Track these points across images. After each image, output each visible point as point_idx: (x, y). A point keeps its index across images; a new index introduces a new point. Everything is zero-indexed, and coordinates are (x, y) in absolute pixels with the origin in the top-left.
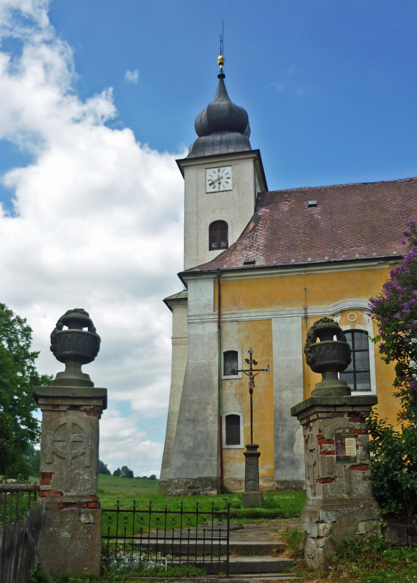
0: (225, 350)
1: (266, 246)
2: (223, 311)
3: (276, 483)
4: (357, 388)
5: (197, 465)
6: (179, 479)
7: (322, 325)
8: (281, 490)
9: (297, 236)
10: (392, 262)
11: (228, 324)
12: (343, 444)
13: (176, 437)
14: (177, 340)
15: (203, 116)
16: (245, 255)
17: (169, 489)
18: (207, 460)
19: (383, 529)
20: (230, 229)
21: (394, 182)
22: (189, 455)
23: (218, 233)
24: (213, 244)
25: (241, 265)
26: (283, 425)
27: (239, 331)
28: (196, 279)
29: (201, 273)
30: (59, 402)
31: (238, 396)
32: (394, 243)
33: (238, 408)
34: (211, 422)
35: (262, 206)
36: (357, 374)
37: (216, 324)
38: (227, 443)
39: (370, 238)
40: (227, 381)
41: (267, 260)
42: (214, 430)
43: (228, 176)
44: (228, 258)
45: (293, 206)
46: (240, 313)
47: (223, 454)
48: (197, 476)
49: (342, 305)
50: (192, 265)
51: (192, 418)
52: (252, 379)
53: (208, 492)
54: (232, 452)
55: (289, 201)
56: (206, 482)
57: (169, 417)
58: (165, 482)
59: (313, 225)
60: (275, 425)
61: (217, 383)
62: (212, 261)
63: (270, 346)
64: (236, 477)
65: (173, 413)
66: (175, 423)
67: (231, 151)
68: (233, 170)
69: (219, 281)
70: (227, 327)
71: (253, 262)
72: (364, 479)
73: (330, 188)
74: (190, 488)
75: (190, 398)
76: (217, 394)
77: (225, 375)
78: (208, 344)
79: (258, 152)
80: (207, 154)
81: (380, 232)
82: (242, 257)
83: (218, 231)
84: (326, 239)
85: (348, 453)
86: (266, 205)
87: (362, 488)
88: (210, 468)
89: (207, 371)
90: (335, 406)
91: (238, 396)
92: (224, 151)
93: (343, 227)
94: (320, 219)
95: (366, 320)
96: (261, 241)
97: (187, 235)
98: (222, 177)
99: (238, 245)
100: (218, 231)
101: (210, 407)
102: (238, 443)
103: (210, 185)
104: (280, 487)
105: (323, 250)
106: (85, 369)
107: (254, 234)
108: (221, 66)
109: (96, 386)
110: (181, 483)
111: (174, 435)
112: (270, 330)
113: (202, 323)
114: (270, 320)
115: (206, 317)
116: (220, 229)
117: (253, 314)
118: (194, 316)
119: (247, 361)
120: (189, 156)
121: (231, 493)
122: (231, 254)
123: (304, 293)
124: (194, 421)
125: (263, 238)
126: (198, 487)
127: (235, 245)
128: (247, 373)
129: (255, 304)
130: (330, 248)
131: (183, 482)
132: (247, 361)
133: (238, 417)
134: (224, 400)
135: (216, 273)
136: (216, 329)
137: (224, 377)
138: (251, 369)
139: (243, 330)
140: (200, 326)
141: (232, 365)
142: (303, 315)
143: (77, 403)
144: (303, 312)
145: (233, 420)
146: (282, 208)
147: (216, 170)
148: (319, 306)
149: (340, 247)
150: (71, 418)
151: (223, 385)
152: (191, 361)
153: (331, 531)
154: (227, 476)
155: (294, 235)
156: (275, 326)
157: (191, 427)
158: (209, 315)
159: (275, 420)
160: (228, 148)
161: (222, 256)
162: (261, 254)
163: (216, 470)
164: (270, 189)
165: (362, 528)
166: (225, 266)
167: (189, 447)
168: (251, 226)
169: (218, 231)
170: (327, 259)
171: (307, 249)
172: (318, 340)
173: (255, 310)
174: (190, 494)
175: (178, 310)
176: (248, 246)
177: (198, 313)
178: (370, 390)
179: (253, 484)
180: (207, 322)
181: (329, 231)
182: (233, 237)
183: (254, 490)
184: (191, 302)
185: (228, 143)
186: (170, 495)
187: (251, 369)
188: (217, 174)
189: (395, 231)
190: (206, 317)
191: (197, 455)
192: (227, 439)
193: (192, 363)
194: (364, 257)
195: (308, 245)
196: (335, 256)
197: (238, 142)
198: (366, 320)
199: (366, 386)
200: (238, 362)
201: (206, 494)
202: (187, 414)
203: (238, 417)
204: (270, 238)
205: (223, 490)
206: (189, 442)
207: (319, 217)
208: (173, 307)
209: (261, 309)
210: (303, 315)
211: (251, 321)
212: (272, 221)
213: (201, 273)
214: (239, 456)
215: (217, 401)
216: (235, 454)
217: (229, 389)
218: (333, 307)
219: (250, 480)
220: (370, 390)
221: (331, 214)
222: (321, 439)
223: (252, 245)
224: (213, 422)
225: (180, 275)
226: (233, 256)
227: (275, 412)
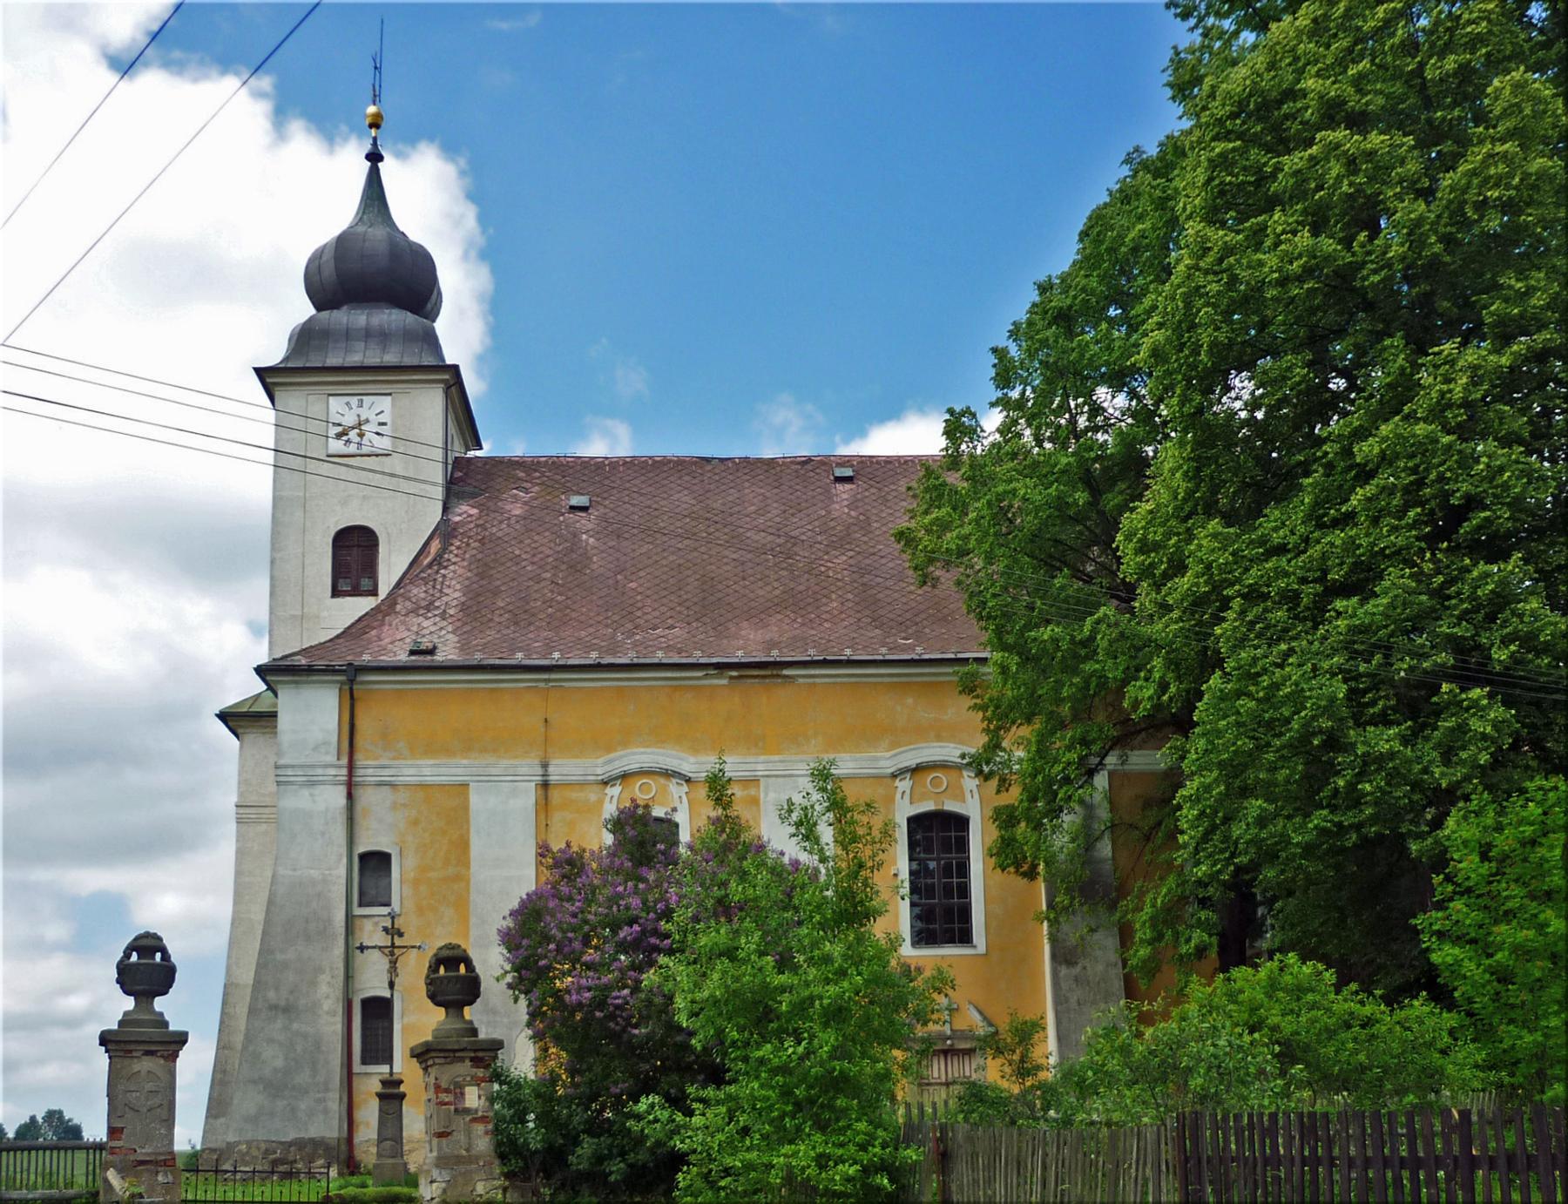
0: (361, 849)
1: (464, 608)
2: (360, 760)
5: (293, 1110)
6: (249, 1143)
7: (445, 953)
10: (734, 673)
11: (370, 791)
12: (463, 1094)
13: (245, 1048)
15: (324, 258)
16: (415, 628)
19: (505, 1190)
22: (276, 1087)
23: (353, 558)
25: (403, 657)
28: (296, 682)
29: (309, 670)
30: (132, 1047)
34: (327, 1013)
35: (462, 496)
37: (342, 790)
38: (364, 1062)
39: (697, 608)
41: (463, 647)
43: (382, 418)
44: (374, 633)
47: (355, 1084)
48: (291, 1135)
49: (625, 761)
50: (292, 644)
51: (283, 1003)
52: (393, 963)
55: (527, 491)
56: (313, 1147)
57: (225, 994)
58: (213, 1150)
59: (574, 560)
61: (343, 924)
62: (338, 637)
63: (463, 845)
65: (237, 985)
66: (242, 1011)
67: (390, 358)
68: (393, 405)
70: (366, 797)
72: (486, 1133)
73: (625, 463)
75: (279, 957)
77: (360, 905)
78: (323, 834)
80: (333, 361)
81: (719, 595)
83: (354, 553)
84: (600, 602)
85: (468, 1105)
87: (483, 1143)
88: (321, 1117)
90: (455, 1051)
92: (373, 359)
93: (642, 574)
95: (676, 796)
96: (453, 595)
97: (278, 556)
98: (367, 421)
99: (400, 600)
100: (354, 553)
101: (324, 978)
103: (339, 436)
105: (591, 630)
106: (159, 1003)
108: (373, 132)
109: (171, 1028)
110: (255, 1152)
111: (238, 1039)
112: (465, 808)
114: (465, 785)
115: (320, 771)
117: (427, 771)
118: (293, 767)
119: (385, 929)
120: (286, 359)
122: (383, 624)
124: (288, 1010)
129: (432, 748)
130: (607, 626)
132: (385, 929)
136: (342, 800)
137: (358, 911)
138: (393, 945)
139: (404, 805)
140: (306, 792)
143: (153, 1048)
144: (540, 771)
146: (508, 507)
147: (354, 401)
149: (629, 626)
150: (145, 1065)
152: (281, 871)
153: (444, 1191)
156: (475, 799)
157: (279, 1024)
158: (326, 766)
160: (384, 350)
161: (359, 626)
163: (336, 1123)
165: (480, 1188)
167: (276, 1070)
171: (556, 623)
172: (442, 971)
173: (432, 762)
175: (254, 737)
176: (423, 603)
177: (302, 760)
180: (323, 783)
181: (611, 582)
182: (391, 566)
184: (283, 721)
185: (383, 337)
187: (393, 945)
188: (356, 410)
189: (752, 595)
190: (320, 771)
192: (364, 1051)
197: (409, 337)
198: (676, 796)
202: (271, 994)
205: (351, 1166)
206: (273, 1058)
213: (309, 670)
215: (341, 965)
218: (606, 763)
222: (438, 1088)
224: (333, 1013)
225: (261, 671)
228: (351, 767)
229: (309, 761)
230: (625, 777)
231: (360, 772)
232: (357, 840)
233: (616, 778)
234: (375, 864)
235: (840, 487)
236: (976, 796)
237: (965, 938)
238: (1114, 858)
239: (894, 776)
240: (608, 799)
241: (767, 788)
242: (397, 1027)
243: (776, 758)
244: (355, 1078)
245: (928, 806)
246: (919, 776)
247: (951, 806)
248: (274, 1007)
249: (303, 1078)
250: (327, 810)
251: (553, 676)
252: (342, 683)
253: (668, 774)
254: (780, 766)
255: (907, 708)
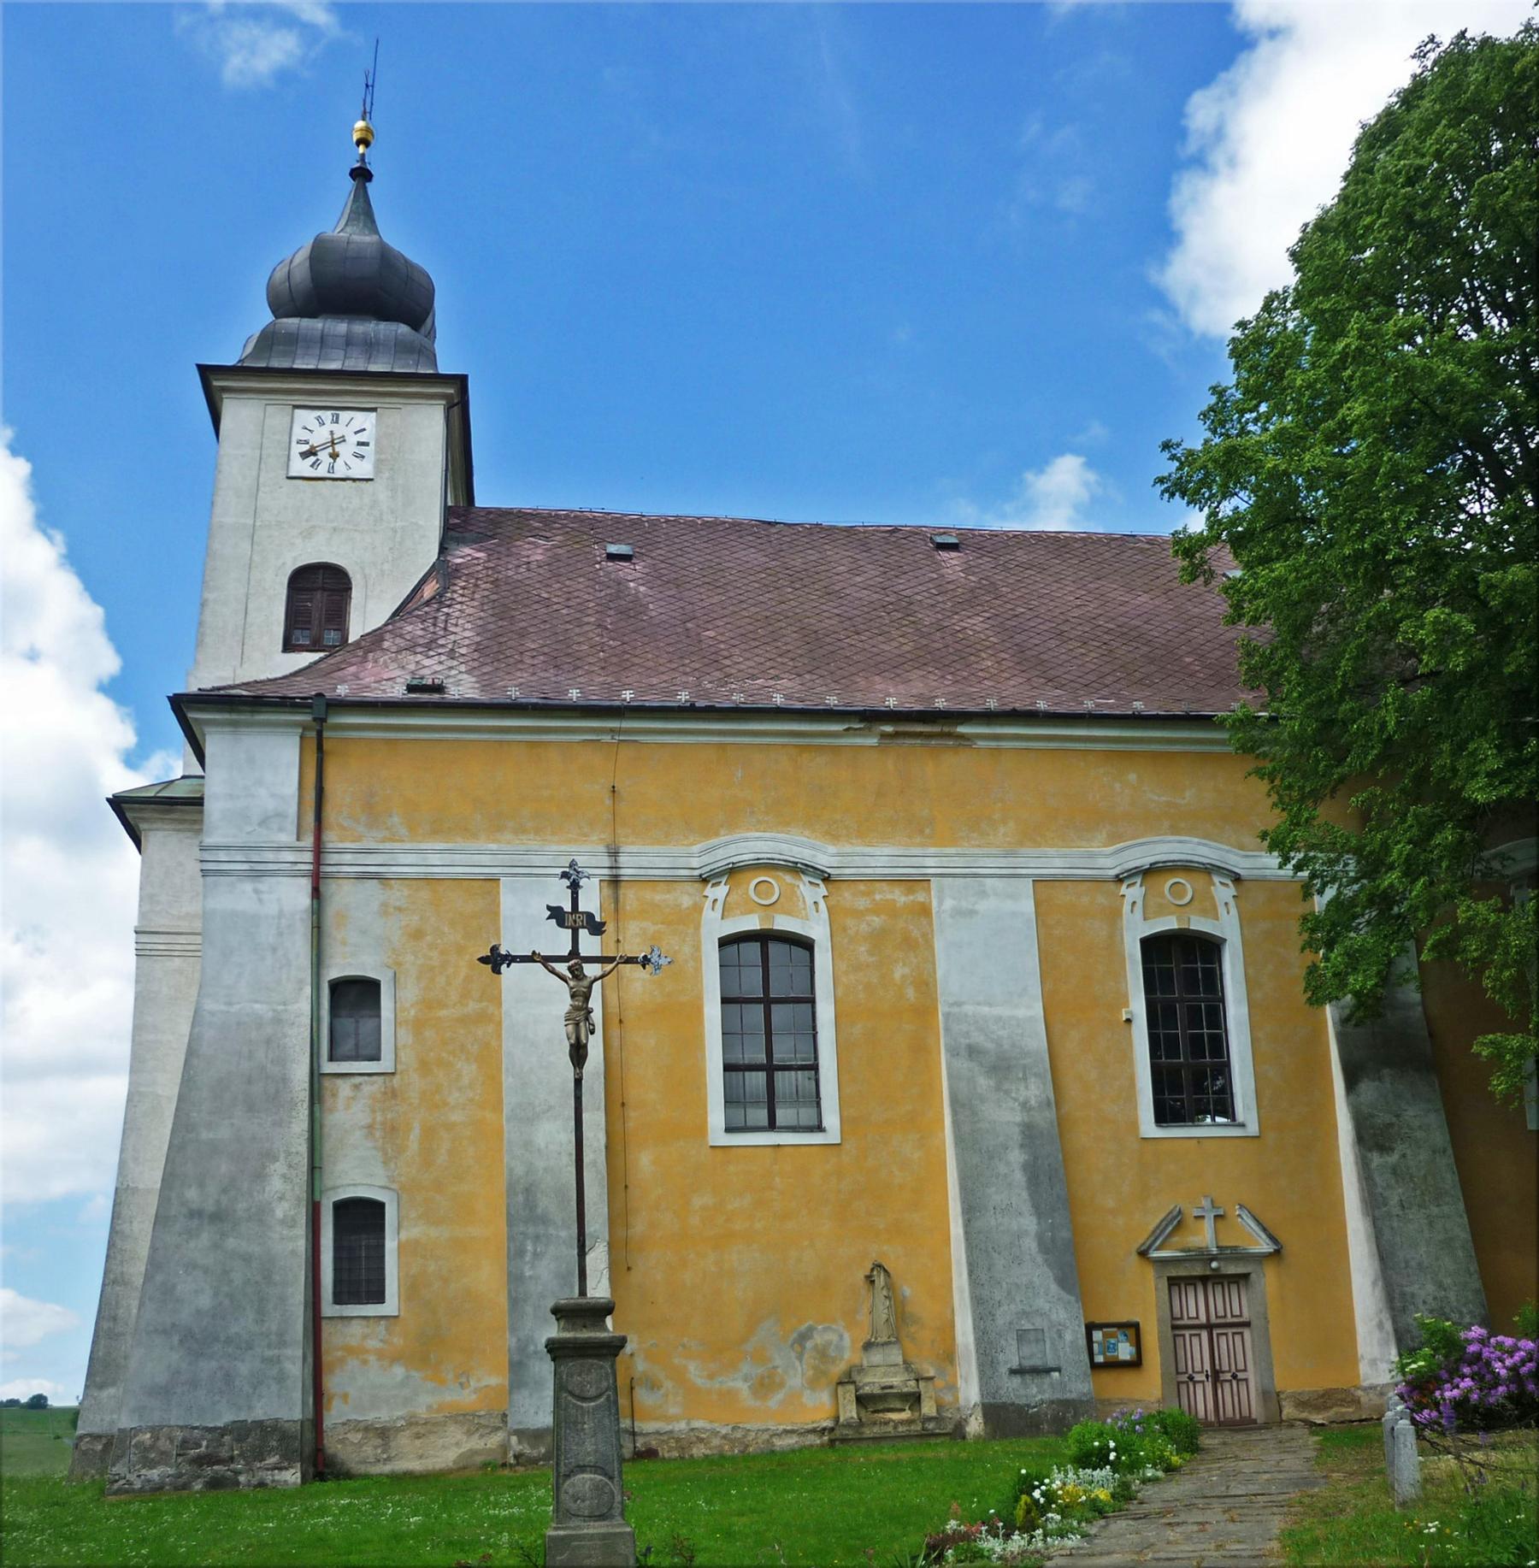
0: (334, 972)
2: (331, 839)
3: (514, 1439)
4: (780, 1121)
5: (228, 1378)
6: (155, 1430)
8: (533, 1461)
9: (577, 630)
10: (889, 729)
13: (148, 1277)
14: (155, 938)
16: (412, 667)
17: (115, 1470)
18: (264, 1360)
20: (356, 594)
21: (850, 531)
22: (196, 1341)
23: (317, 603)
24: (297, 632)
25: (397, 692)
26: (537, 1238)
27: (384, 910)
28: (235, 724)
31: (378, 1134)
32: (877, 678)
33: (380, 1175)
34: (283, 1222)
35: (462, 541)
36: (778, 1075)
37: (305, 884)
38: (338, 1299)
40: (339, 1082)
42: (293, 1253)
43: (362, 437)
44: (353, 669)
45: (560, 551)
46: (391, 852)
47: (324, 1335)
48: (226, 1417)
51: (210, 1207)
53: (268, 1477)
54: (356, 1329)
56: (259, 1438)
57: (117, 1204)
60: (511, 1238)
61: (307, 1085)
64: (370, 1416)
66: (142, 1228)
69: (320, 734)
70: (341, 895)
71: (439, 689)
73: (667, 521)
74: (200, 1461)
75: (205, 1135)
76: (305, 1125)
77: (331, 1059)
78: (274, 950)
79: (461, 381)
80: (275, 364)
82: (398, 673)
86: (478, 540)
88: (274, 1387)
89: (268, 1042)
91: (378, 1134)
93: (719, 623)
94: (646, 596)
95: (809, 902)
96: (464, 633)
99: (388, 636)
101: (279, 1167)
102: (379, 1297)
103: (305, 455)
104: (528, 1451)
105: (665, 677)
107: (438, 610)
110: (164, 1444)
111: (137, 1270)
113: (257, 875)
115: (270, 856)
116: (324, 589)
117: (434, 859)
118: (227, 848)
119: (556, 914)
121: (349, 1476)
122: (365, 660)
123: (608, 802)
125: (469, 626)
126: (232, 1459)
127: (374, 640)
128: (562, 968)
130: (686, 674)
131: (171, 1440)
132: (556, 914)
133: (377, 1208)
134: (328, 1146)
135: (314, 715)
137: (329, 1067)
140: (248, 886)
141: (357, 1028)
142: (606, 871)
144: (606, 861)
145: (360, 1219)
147: (327, 415)
148: (656, 848)
149: (718, 674)
151: (327, 1095)
152: (209, 1005)
154: (333, 1416)
155: (568, 626)
157: (205, 1238)
158: (279, 849)
159: (510, 1224)
162: (463, 668)
163: (297, 1395)
164: (479, 502)
166: (342, 691)
167: (198, 1312)
168: (429, 591)
169: (318, 595)
170: (683, 697)
174: (198, 1486)
177: (239, 841)
178: (819, 1128)
179: (598, 1488)
182: (367, 613)
183: (602, 1517)
186: (117, 1492)
187: (574, 952)
188: (329, 426)
190: (270, 856)
191: (229, 1341)
192: (337, 1282)
193: (212, 1014)
194: (799, 705)
195: (614, 660)
196: (706, 694)
198: (809, 902)
199: (806, 1115)
200: (379, 1016)
201: (262, 1484)
202: (192, 1194)
203: (377, 1208)
204: (492, 626)
206: (196, 1295)
207: (642, 589)
208: (143, 826)
209: (461, 844)
210: (606, 871)
211: (428, 880)
212: (495, 582)
214: (379, 1345)
215: (303, 1148)
216: (365, 1337)
217: (347, 1107)
218: (703, 853)
219: (582, 1468)
220: (819, 1128)
221: (678, 586)
223: (434, 641)
224: (288, 1222)
226: (370, 665)
227: (511, 1189)
228: (319, 850)
229: (251, 840)
230: (733, 871)
231: (332, 858)
232: (327, 961)
233: (720, 874)
234: (354, 997)
235: (944, 555)
236: (1234, 911)
237: (1224, 1107)
238: (1423, 1003)
239: (1119, 880)
240: (708, 903)
241: (941, 891)
242: (391, 1245)
243: (952, 850)
244: (325, 1325)
245: (1169, 923)
246: (1155, 880)
247: (1199, 924)
248: (195, 1214)
249: (243, 1325)
250: (281, 914)
251: (626, 724)
252: (305, 728)
253: (798, 869)
254: (960, 862)
255: (1131, 786)
